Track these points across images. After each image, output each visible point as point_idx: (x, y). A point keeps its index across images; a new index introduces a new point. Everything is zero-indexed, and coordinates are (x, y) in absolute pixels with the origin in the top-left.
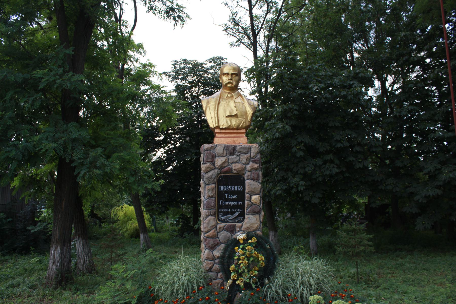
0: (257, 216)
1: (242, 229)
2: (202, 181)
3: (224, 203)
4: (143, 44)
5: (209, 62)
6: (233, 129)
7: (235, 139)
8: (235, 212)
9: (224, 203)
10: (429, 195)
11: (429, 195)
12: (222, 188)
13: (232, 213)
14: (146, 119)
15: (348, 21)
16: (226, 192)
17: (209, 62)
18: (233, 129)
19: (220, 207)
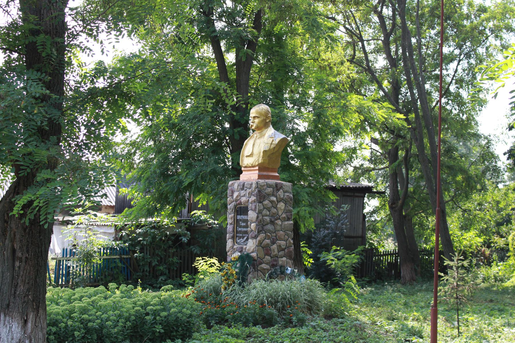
0: (255, 240)
1: (262, 245)
2: (351, 186)
3: (240, 229)
4: (488, 105)
5: (509, 130)
6: (250, 167)
7: (251, 175)
8: (244, 237)
9: (240, 229)
10: (144, 289)
11: (144, 289)
12: (239, 217)
13: (243, 237)
14: (132, 110)
15: (196, 95)
16: (240, 220)
17: (509, 130)
18: (250, 167)
19: (237, 232)
